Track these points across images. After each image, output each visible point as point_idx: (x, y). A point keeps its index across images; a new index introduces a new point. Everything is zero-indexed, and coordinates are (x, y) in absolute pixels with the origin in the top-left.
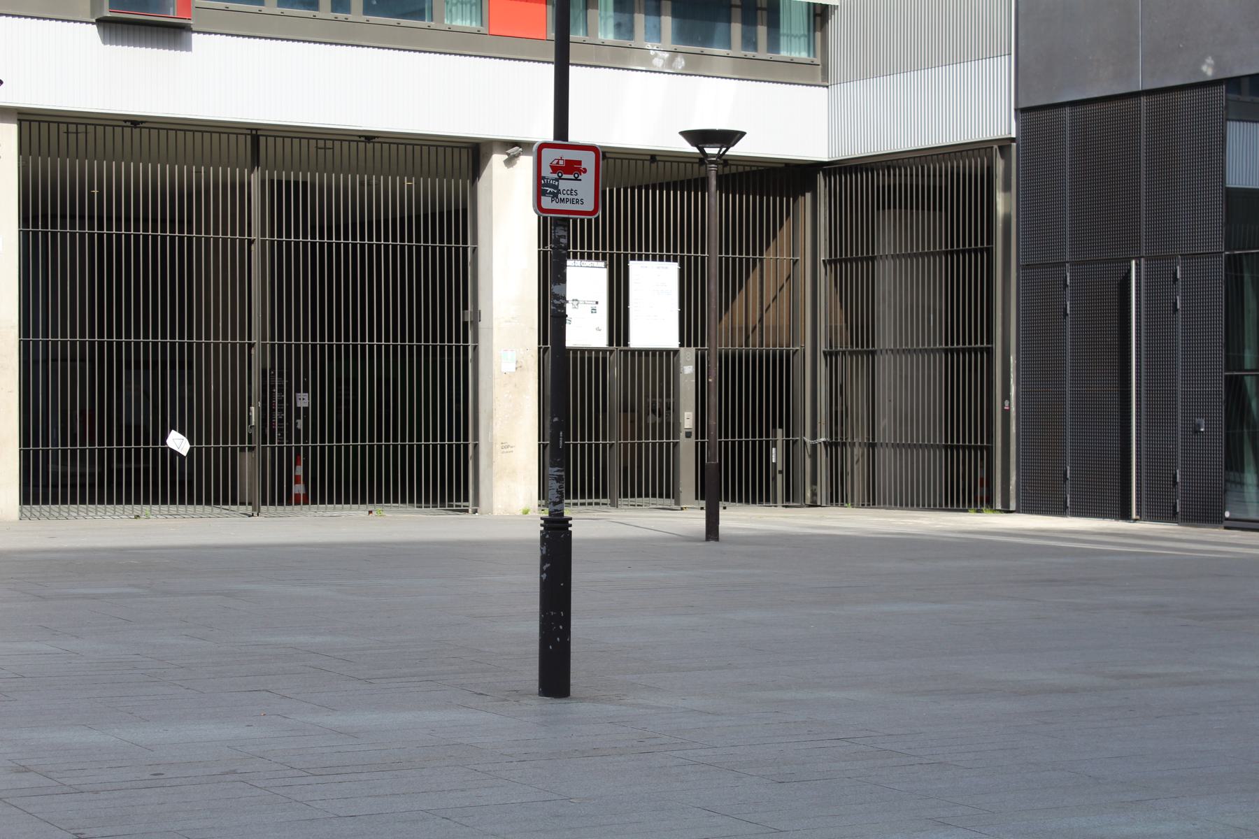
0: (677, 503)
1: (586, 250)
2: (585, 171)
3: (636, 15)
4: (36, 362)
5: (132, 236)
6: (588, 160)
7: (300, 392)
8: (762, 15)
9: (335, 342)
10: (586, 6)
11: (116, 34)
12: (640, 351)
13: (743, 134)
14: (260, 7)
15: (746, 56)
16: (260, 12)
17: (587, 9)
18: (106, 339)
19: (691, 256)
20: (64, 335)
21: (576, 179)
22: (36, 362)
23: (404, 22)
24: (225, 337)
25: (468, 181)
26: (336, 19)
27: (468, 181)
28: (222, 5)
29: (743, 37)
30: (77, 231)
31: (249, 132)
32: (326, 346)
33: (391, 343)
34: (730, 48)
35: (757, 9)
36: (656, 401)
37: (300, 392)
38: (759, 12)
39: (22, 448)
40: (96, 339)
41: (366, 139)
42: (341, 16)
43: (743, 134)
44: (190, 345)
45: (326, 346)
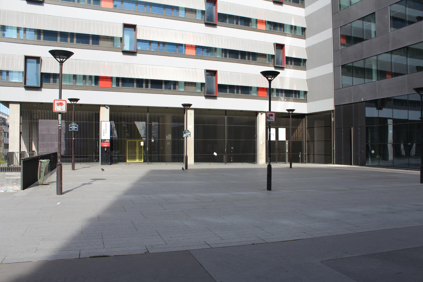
2: (64, 104)
13: (295, 110)
21: (62, 106)
43: (295, 110)
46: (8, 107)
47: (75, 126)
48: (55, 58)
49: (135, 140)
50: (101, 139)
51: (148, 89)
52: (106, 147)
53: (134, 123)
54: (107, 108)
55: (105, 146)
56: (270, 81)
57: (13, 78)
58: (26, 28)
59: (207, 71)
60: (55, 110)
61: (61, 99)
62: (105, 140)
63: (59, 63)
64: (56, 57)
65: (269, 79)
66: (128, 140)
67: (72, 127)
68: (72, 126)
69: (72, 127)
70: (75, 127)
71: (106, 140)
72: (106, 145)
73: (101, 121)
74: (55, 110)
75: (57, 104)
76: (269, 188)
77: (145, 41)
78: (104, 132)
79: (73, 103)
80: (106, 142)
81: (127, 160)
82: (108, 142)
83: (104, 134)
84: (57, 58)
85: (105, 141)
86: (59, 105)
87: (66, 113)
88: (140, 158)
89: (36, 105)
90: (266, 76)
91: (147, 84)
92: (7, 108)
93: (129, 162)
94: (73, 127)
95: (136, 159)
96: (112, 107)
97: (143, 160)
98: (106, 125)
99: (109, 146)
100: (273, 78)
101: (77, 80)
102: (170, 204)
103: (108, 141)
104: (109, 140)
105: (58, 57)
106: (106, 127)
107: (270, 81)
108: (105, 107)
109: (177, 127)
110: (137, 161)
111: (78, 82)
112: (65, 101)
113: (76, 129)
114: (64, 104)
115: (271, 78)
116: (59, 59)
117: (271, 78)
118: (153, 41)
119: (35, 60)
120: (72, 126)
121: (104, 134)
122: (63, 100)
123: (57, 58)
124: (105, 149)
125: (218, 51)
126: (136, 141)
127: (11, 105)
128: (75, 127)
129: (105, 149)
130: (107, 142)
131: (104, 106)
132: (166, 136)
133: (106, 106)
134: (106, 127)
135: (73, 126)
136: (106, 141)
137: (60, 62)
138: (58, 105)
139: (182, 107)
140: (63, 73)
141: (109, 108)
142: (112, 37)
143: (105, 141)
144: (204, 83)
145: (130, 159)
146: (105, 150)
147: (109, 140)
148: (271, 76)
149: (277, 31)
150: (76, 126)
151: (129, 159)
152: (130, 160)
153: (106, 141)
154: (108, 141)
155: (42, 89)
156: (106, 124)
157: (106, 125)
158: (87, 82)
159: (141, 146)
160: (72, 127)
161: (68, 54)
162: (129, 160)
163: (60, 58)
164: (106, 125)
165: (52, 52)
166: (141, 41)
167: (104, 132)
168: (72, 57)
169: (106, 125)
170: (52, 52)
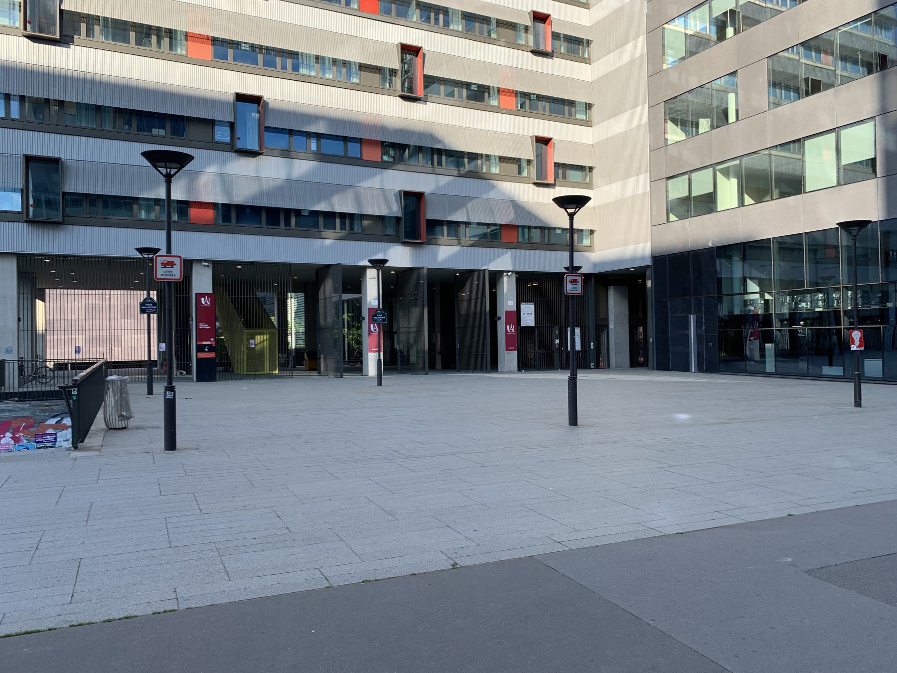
0: (319, 373)
2: (176, 264)
6: (177, 261)
12: (526, 327)
13: (581, 267)
21: (172, 267)
43: (581, 267)
47: (151, 305)
48: (156, 167)
53: (256, 295)
56: (571, 216)
58: (214, 120)
59: (29, 160)
60: (159, 276)
61: (171, 253)
63: (163, 179)
64: (157, 164)
65: (570, 211)
67: (146, 307)
68: (146, 305)
70: (382, 318)
74: (159, 276)
75: (162, 264)
76: (573, 420)
77: (305, 133)
79: (146, 256)
84: (159, 169)
86: (167, 267)
87: (180, 282)
90: (565, 206)
96: (216, 265)
100: (577, 209)
102: (409, 459)
105: (163, 164)
107: (571, 216)
112: (179, 259)
113: (384, 320)
114: (176, 264)
115: (574, 209)
116: (163, 171)
117: (574, 209)
118: (350, 138)
119: (414, 198)
120: (146, 305)
122: (174, 255)
123: (159, 169)
125: (493, 160)
128: (382, 318)
135: (148, 303)
137: (165, 176)
138: (165, 267)
139: (138, 255)
140: (574, 228)
144: (400, 217)
148: (575, 206)
149: (537, 112)
150: (384, 315)
160: (146, 307)
161: (183, 160)
163: (166, 168)
165: (147, 155)
166: (298, 132)
168: (189, 167)
170: (147, 155)
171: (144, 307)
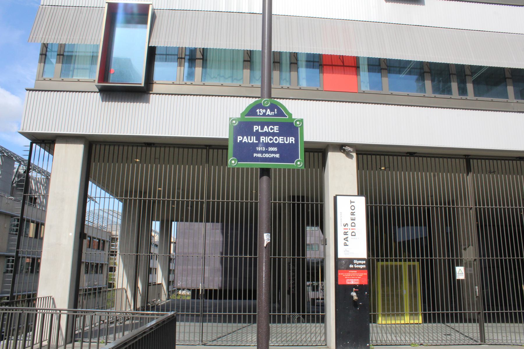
1: (443, 206)
3: (508, 87)
4: (485, 268)
5: (301, 204)
7: (316, 285)
8: (199, 62)
9: (425, 258)
10: (41, 61)
11: (112, 100)
14: (451, 96)
15: (461, 98)
16: (451, 98)
17: (382, 77)
18: (301, 257)
19: (295, 203)
20: (231, 254)
22: (485, 268)
23: (495, 99)
24: (440, 256)
25: (465, 174)
26: (461, 99)
27: (465, 174)
28: (406, 93)
29: (459, 88)
30: (277, 202)
31: (464, 157)
32: (425, 260)
33: (385, 258)
34: (425, 92)
35: (465, 75)
36: (391, 292)
37: (316, 285)
38: (451, 76)
39: (423, 312)
40: (253, 256)
41: (410, 154)
42: (464, 97)
44: (279, 259)
45: (425, 260)
46: (51, 151)
47: (276, 129)
49: (398, 263)
50: (337, 260)
51: (466, 99)
52: (354, 286)
54: (348, 154)
55: (352, 282)
57: (75, 71)
62: (351, 261)
66: (380, 263)
69: (258, 135)
70: (280, 140)
71: (355, 262)
72: (355, 277)
73: (335, 198)
78: (346, 233)
80: (354, 269)
81: (380, 318)
82: (361, 267)
83: (346, 239)
85: (351, 266)
88: (413, 313)
89: (141, 160)
91: (462, 85)
92: (47, 153)
93: (384, 322)
94: (263, 139)
95: (403, 315)
97: (420, 317)
98: (353, 208)
99: (365, 282)
101: (254, 70)
103: (360, 264)
104: (364, 262)
106: (353, 214)
108: (344, 151)
109: (421, 239)
110: (407, 319)
111: (257, 80)
120: (256, 128)
121: (346, 239)
124: (354, 294)
126: (401, 266)
127: (58, 147)
128: (280, 140)
129: (354, 294)
130: (359, 269)
131: (341, 147)
132: (463, 251)
133: (348, 148)
134: (353, 214)
135: (262, 124)
136: (356, 266)
141: (354, 155)
142: (314, 54)
143: (351, 266)
145: (388, 315)
146: (352, 297)
147: (364, 262)
151: (383, 315)
152: (393, 318)
153: (353, 264)
154: (360, 264)
155: (151, 95)
156: (352, 204)
157: (353, 208)
158: (285, 79)
159: (459, 280)
160: (253, 140)
162: (383, 318)
164: (353, 208)
167: (346, 233)
169: (353, 208)
171: (245, 139)
